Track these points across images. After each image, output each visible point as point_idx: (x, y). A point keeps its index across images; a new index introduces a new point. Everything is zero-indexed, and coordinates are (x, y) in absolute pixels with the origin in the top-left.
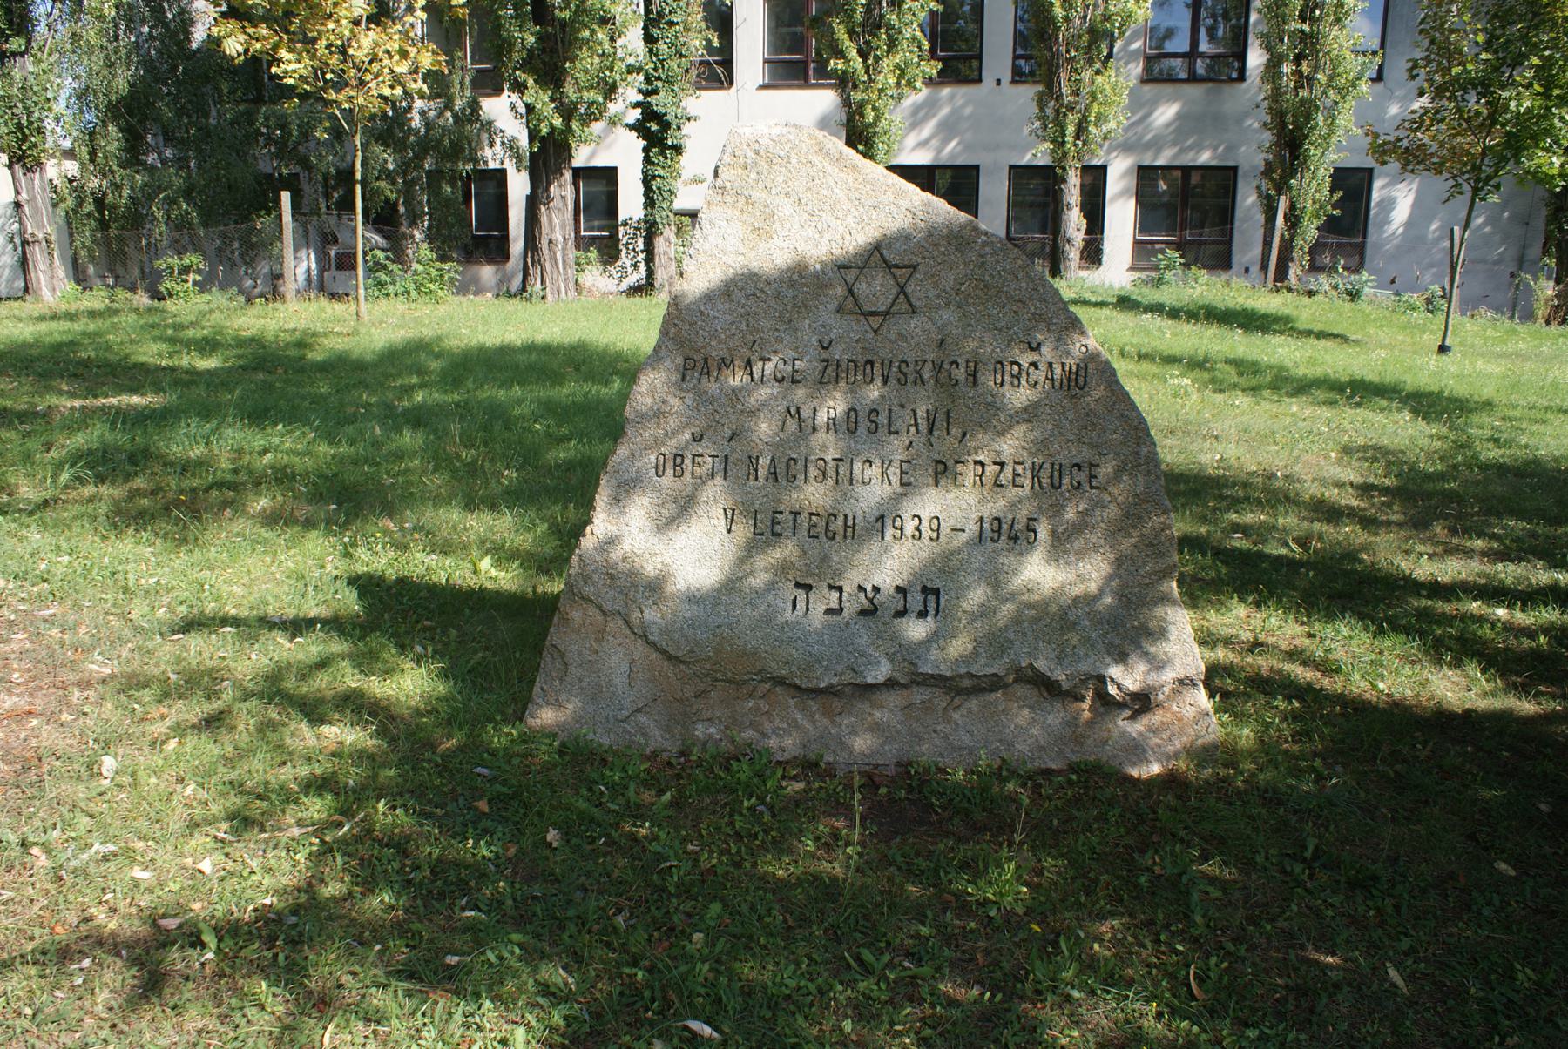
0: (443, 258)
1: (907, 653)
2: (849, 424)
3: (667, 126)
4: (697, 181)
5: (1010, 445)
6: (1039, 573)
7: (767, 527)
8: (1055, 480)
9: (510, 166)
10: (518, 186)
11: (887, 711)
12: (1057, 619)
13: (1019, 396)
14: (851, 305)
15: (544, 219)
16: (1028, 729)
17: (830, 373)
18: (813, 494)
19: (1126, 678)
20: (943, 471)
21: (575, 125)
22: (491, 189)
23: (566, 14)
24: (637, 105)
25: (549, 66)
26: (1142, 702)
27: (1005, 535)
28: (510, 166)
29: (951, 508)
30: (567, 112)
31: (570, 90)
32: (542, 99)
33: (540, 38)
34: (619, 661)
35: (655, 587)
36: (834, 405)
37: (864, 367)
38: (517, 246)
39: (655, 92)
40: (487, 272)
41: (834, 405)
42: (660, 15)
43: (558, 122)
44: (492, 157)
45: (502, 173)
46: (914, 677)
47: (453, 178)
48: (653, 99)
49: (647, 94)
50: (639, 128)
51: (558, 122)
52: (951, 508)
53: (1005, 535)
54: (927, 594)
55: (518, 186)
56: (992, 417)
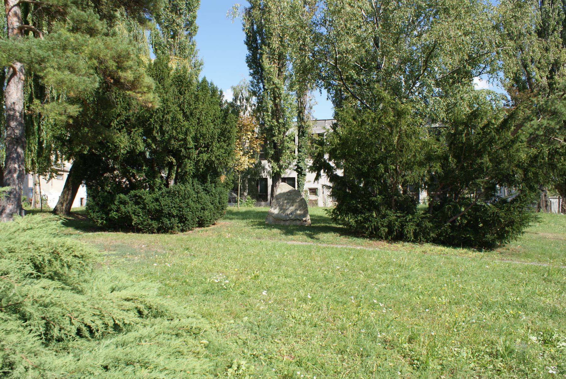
0: (252, 199)
1: (290, 218)
2: (287, 203)
3: (302, 170)
4: (309, 182)
5: (297, 204)
6: (298, 212)
7: (281, 209)
8: (300, 206)
9: (268, 177)
10: (270, 182)
11: (289, 222)
12: (300, 215)
13: (298, 201)
14: (287, 195)
15: (275, 190)
16: (298, 223)
17: (286, 199)
18: (284, 207)
19: (304, 219)
20: (293, 206)
21: (282, 170)
22: (264, 183)
23: (280, 148)
24: (296, 165)
25: (276, 158)
26: (305, 221)
27: (296, 210)
28: (268, 177)
29: (292, 208)
30: (280, 167)
31: (281, 163)
32: (275, 165)
33: (275, 152)
34: (271, 218)
35: (274, 214)
36: (286, 202)
37: (288, 199)
38: (269, 197)
39: (300, 162)
40: (263, 203)
41: (286, 202)
42: (301, 146)
43: (278, 170)
44: (264, 175)
45: (266, 179)
46: (291, 219)
47: (254, 180)
48: (299, 164)
49: (298, 163)
50: (296, 170)
51: (278, 170)
52: (292, 208)
53: (296, 210)
54: (291, 214)
55: (270, 182)
56: (296, 202)
